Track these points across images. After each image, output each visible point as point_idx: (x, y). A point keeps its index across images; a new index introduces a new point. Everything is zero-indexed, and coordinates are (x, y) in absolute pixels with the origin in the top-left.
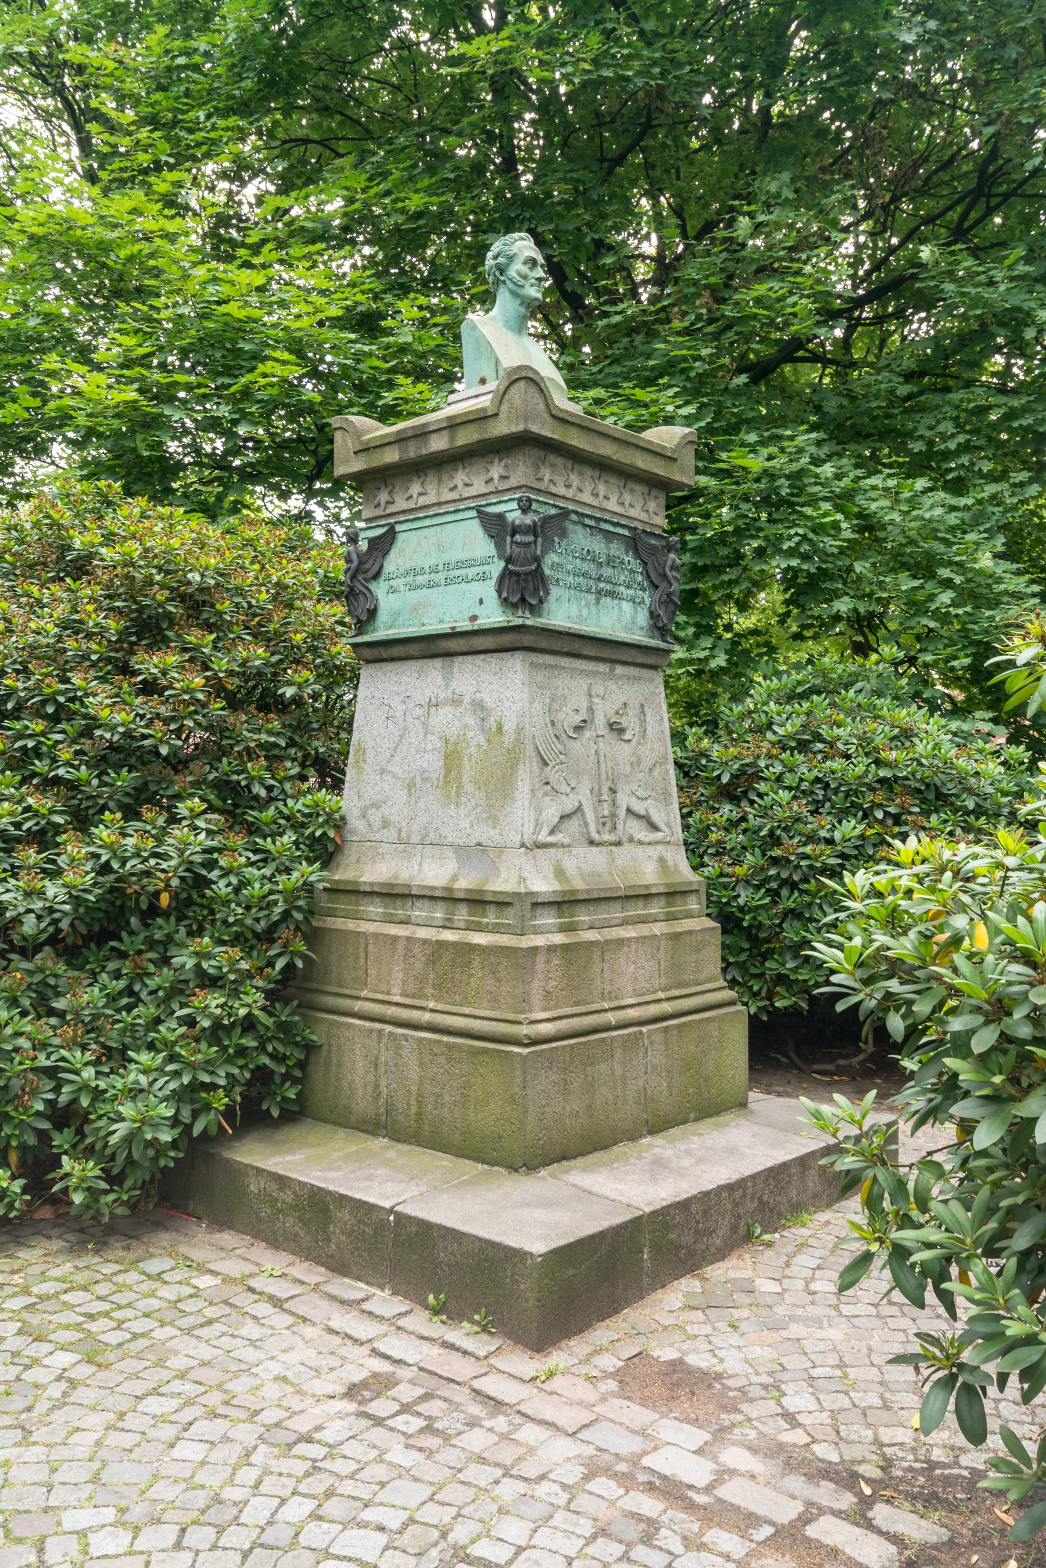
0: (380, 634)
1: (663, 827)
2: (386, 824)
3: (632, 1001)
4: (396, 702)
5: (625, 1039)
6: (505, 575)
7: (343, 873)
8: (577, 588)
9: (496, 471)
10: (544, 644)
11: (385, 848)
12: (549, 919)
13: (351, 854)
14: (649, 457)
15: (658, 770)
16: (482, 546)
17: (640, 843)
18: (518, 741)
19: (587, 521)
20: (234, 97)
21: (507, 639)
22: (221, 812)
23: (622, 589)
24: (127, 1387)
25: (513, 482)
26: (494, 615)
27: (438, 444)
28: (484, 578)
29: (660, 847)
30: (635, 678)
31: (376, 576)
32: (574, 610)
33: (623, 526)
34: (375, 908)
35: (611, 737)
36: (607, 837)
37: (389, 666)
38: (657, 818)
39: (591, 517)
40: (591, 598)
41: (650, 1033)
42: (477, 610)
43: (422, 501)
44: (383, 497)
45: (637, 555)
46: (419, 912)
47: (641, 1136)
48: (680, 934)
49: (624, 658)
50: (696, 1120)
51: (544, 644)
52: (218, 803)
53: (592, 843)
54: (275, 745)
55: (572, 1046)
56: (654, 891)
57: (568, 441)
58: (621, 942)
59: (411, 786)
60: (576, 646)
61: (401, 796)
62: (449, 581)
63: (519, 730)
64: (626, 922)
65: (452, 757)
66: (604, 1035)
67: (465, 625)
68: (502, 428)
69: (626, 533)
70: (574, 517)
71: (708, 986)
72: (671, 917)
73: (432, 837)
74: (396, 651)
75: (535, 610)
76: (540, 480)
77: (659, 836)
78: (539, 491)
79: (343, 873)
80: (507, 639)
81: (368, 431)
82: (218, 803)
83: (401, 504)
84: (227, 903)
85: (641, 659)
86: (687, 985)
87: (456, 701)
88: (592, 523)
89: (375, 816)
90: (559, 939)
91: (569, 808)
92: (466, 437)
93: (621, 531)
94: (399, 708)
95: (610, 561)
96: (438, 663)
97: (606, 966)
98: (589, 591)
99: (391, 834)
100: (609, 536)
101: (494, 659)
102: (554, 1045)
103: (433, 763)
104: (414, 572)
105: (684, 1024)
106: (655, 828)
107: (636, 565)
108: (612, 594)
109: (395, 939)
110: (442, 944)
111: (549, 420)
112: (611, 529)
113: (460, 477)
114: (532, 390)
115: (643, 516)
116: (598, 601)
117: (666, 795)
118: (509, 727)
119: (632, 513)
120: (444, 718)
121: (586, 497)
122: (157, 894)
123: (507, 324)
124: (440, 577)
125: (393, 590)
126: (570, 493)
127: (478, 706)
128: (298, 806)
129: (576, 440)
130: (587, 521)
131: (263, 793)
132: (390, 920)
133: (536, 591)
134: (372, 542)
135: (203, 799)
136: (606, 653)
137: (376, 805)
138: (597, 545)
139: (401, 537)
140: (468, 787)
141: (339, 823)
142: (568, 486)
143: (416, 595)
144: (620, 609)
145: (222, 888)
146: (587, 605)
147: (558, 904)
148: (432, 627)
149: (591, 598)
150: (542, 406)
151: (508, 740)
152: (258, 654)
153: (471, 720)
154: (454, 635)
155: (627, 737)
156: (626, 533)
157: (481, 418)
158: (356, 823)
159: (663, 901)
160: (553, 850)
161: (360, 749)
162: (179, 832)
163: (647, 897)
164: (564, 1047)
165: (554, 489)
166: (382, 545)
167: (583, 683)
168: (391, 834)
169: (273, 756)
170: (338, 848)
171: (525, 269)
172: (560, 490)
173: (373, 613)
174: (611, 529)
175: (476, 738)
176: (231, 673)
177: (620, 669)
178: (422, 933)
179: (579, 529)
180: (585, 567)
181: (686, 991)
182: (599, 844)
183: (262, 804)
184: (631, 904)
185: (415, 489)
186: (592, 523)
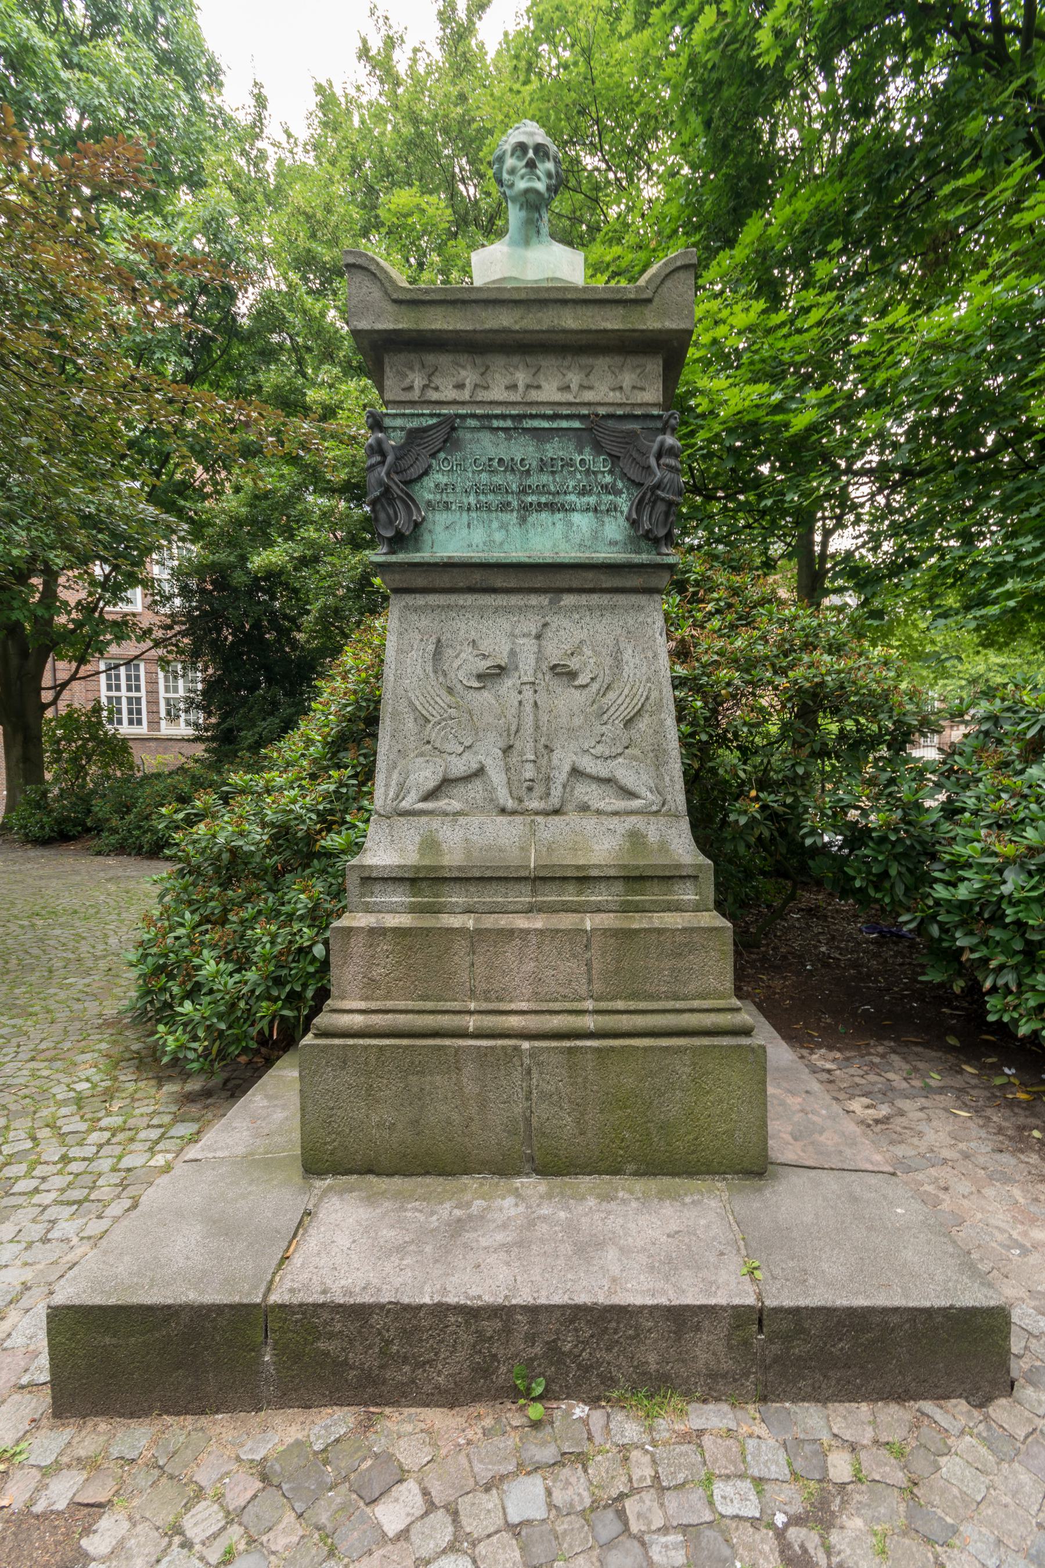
1: (643, 791)
3: (524, 1006)
5: (482, 1054)
10: (420, 582)
12: (398, 897)
14: (589, 311)
15: (643, 724)
17: (599, 812)
19: (495, 423)
23: (572, 498)
24: (863, 1081)
29: (633, 819)
30: (601, 608)
32: (478, 536)
33: (568, 417)
35: (557, 685)
36: (535, 805)
38: (627, 777)
39: (504, 417)
40: (512, 518)
41: (533, 1053)
45: (598, 448)
47: (518, 1174)
48: (636, 932)
49: (575, 584)
50: (636, 1174)
51: (420, 582)
53: (503, 811)
55: (381, 1048)
56: (594, 873)
57: (425, 326)
58: (509, 934)
60: (477, 578)
64: (530, 910)
66: (447, 1042)
69: (576, 424)
70: (472, 423)
71: (696, 1004)
72: (626, 908)
76: (410, 388)
77: (636, 803)
78: (412, 403)
85: (608, 582)
86: (651, 997)
88: (509, 423)
90: (404, 920)
91: (459, 767)
93: (564, 424)
97: (479, 960)
98: (505, 507)
102: (351, 1042)
105: (612, 1049)
106: (632, 795)
107: (600, 464)
111: (390, 307)
112: (545, 424)
114: (359, 277)
116: (523, 520)
117: (659, 756)
119: (588, 396)
121: (497, 393)
126: (465, 395)
129: (438, 321)
130: (495, 423)
136: (539, 581)
142: (460, 386)
144: (569, 524)
146: (504, 526)
147: (413, 881)
149: (512, 518)
150: (377, 294)
155: (581, 680)
156: (576, 424)
159: (619, 887)
160: (424, 819)
163: (584, 879)
164: (366, 1048)
165: (434, 396)
167: (504, 623)
174: (545, 424)
177: (568, 600)
179: (486, 437)
180: (497, 479)
181: (642, 1005)
182: (514, 813)
184: (547, 887)
186: (509, 423)
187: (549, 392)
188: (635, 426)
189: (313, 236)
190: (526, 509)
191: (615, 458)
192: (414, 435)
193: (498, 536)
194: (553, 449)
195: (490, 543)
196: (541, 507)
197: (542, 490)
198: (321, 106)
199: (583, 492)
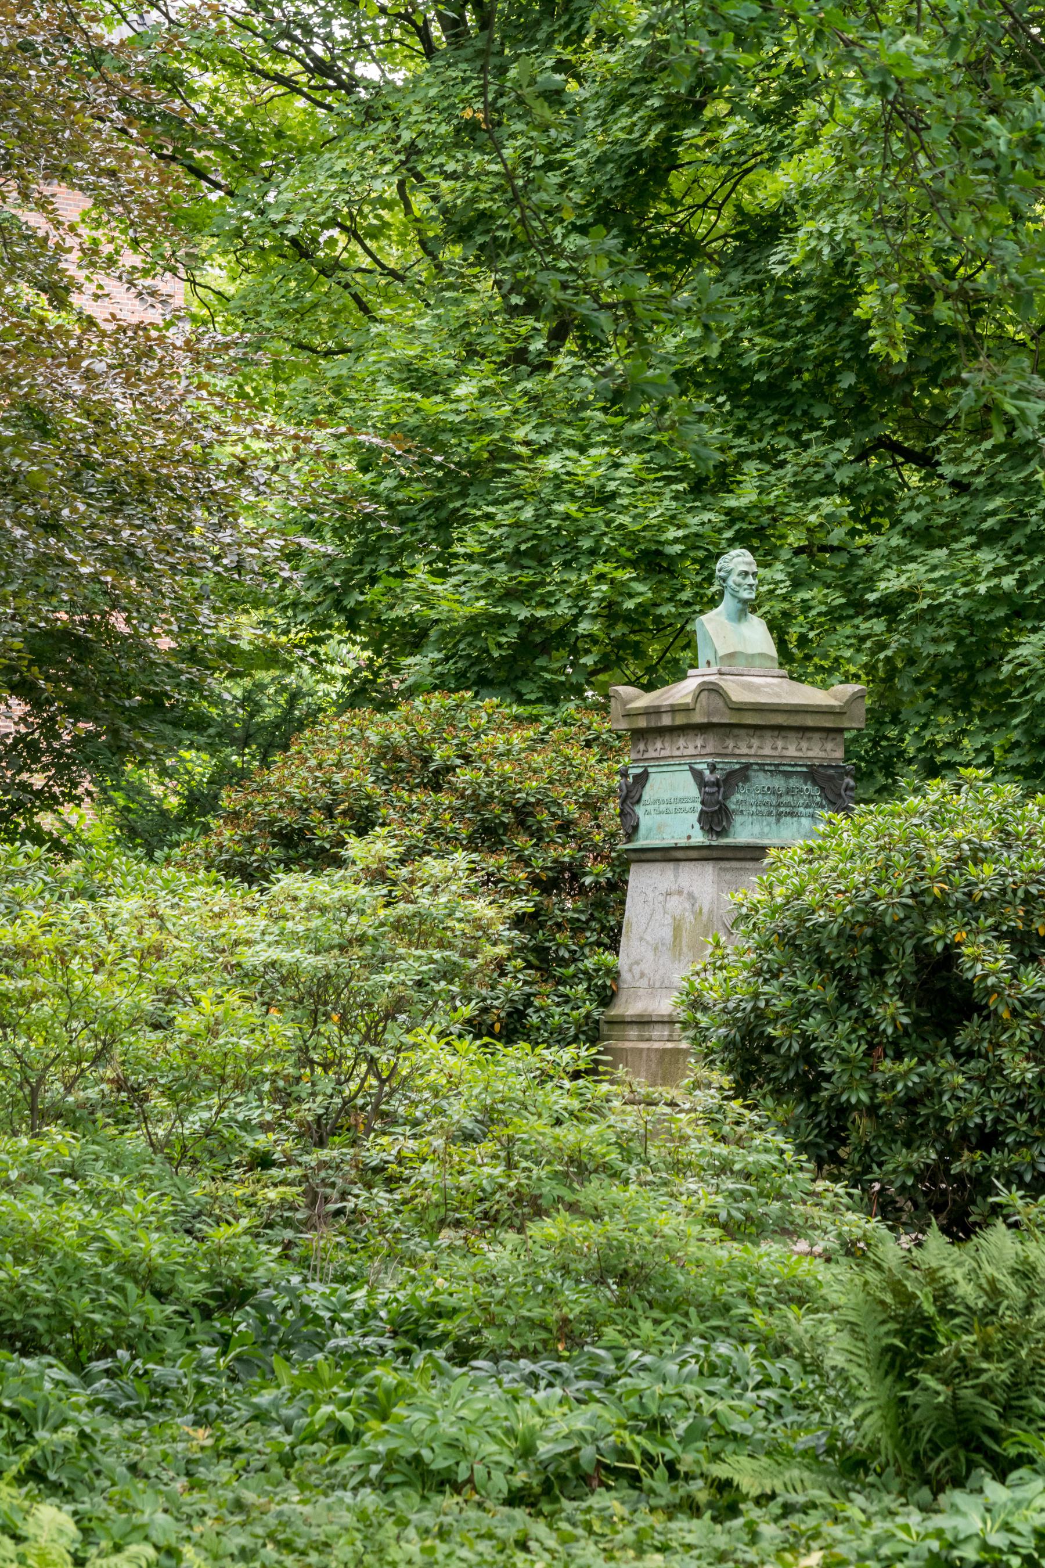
0: (640, 843)
2: (642, 975)
4: (649, 891)
6: (702, 812)
7: (616, 1011)
8: (760, 814)
9: (699, 742)
10: (730, 855)
11: (641, 992)
13: (622, 997)
14: (817, 717)
16: (692, 790)
18: (710, 920)
20: (435, 962)
21: (705, 853)
22: (538, 969)
25: (708, 750)
26: (699, 838)
27: (666, 721)
28: (693, 811)
31: (638, 801)
32: (756, 829)
34: (633, 1032)
37: (646, 866)
40: (773, 819)
42: (690, 832)
43: (664, 753)
44: (641, 746)
45: (815, 783)
46: (657, 1032)
51: (730, 855)
52: (535, 962)
54: (578, 920)
59: (656, 949)
61: (650, 955)
62: (677, 811)
63: (711, 912)
65: (677, 929)
67: (683, 842)
68: (698, 718)
73: (666, 983)
74: (649, 856)
75: (723, 833)
78: (726, 755)
79: (614, 1012)
80: (705, 853)
81: (632, 701)
82: (535, 962)
83: (651, 754)
84: (538, 1029)
87: (680, 892)
89: (636, 969)
92: (680, 720)
94: (651, 895)
95: (789, 791)
96: (671, 865)
98: (770, 814)
99: (644, 983)
100: (787, 775)
101: (698, 864)
103: (667, 933)
104: (657, 801)
107: (816, 791)
108: (792, 814)
109: (641, 1050)
110: (665, 1050)
113: (681, 742)
114: (713, 695)
115: (822, 754)
118: (705, 910)
119: (810, 754)
120: (674, 902)
121: (767, 751)
122: (492, 1025)
123: (730, 618)
124: (672, 807)
125: (647, 813)
126: (752, 752)
127: (691, 896)
128: (589, 964)
131: (567, 955)
132: (642, 1039)
133: (720, 823)
134: (636, 777)
135: (525, 960)
137: (637, 963)
138: (778, 783)
139: (652, 776)
140: (685, 949)
141: (614, 974)
143: (659, 818)
145: (535, 1019)
148: (669, 842)
149: (773, 819)
150: (721, 704)
151: (705, 918)
152: (567, 853)
153: (687, 905)
154: (676, 848)
157: (686, 709)
158: (625, 975)
161: (630, 924)
162: (506, 981)
166: (642, 779)
168: (644, 983)
169: (578, 928)
170: (614, 994)
171: (739, 580)
172: (744, 750)
173: (636, 828)
175: (690, 917)
176: (544, 869)
178: (656, 1045)
179: (761, 774)
180: (766, 799)
183: (563, 962)
185: (659, 745)
187: (792, 751)
188: (831, 771)
189: (436, 1096)
190: (779, 815)
191: (822, 789)
192: (731, 774)
193: (766, 830)
194: (794, 782)
195: (762, 835)
196: (787, 814)
197: (788, 805)
198: (478, 1036)
199: (807, 806)
